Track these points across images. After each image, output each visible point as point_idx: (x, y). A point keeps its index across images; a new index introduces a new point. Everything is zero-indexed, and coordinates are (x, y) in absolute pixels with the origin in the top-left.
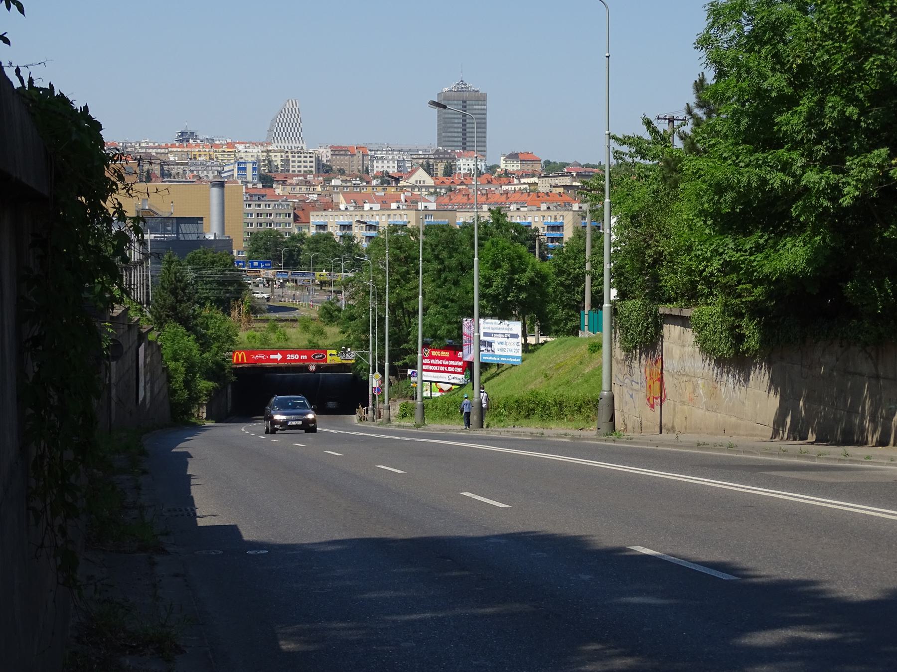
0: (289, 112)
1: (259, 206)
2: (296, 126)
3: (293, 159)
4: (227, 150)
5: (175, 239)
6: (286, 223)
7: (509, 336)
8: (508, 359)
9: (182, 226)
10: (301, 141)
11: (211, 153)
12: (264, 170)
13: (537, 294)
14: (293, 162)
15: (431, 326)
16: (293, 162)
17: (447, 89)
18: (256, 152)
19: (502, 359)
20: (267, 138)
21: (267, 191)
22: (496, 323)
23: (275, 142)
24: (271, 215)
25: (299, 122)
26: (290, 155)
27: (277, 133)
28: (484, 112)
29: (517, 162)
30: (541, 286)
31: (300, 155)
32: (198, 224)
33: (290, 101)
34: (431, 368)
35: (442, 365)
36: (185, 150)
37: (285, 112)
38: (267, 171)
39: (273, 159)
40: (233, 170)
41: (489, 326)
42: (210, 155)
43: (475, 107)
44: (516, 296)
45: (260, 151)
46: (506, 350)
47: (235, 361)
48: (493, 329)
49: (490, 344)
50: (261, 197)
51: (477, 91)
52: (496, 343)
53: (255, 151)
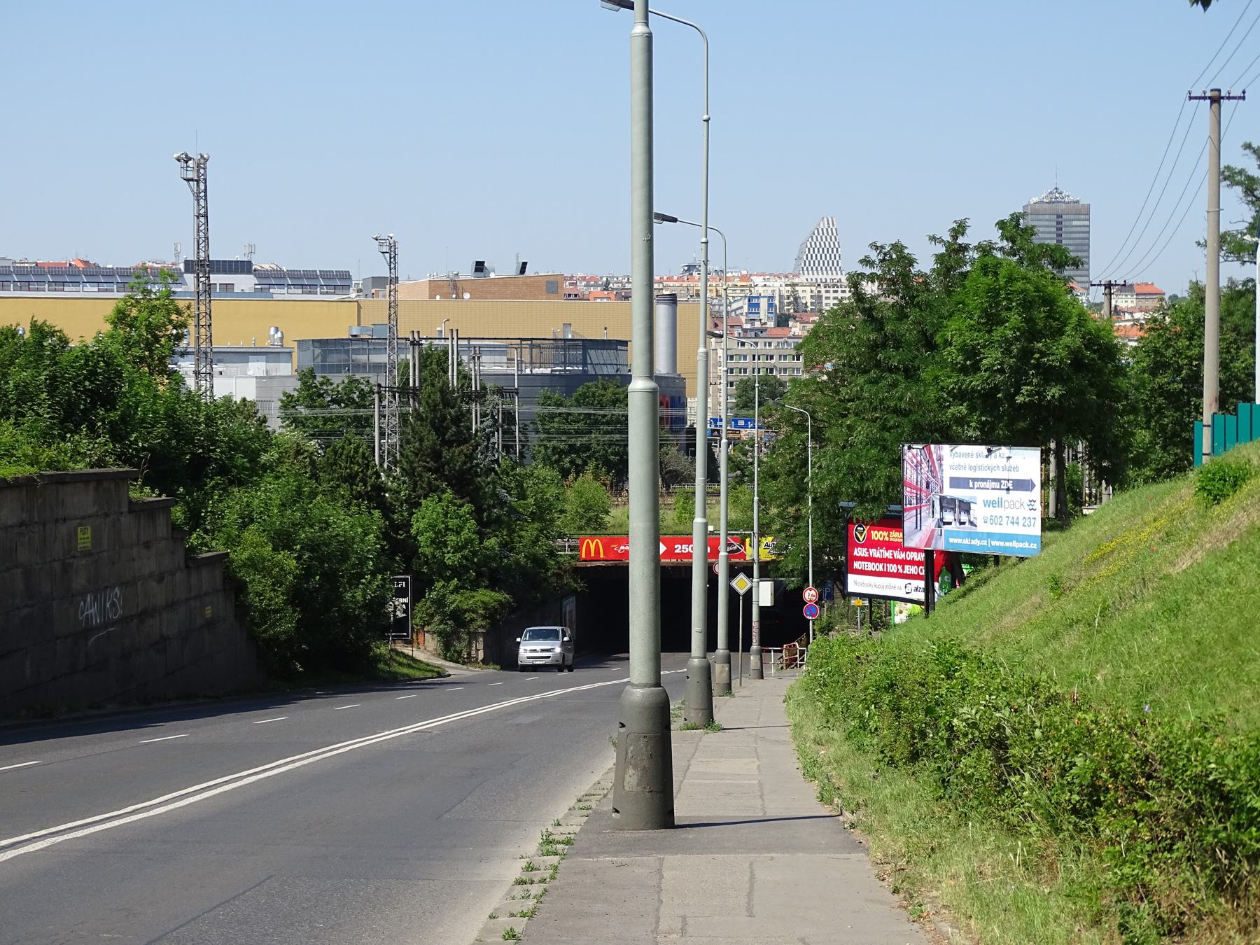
0: (823, 234)
1: (756, 344)
2: (833, 252)
3: (828, 295)
4: (739, 284)
5: (580, 373)
6: (767, 356)
7: (1010, 485)
8: (1008, 544)
9: (592, 352)
10: (839, 272)
11: (718, 288)
12: (789, 310)
13: (1090, 389)
14: (827, 298)
15: (851, 470)
16: (827, 298)
17: (1035, 200)
18: (778, 286)
19: (994, 543)
20: (795, 269)
21: (780, 331)
22: (979, 455)
23: (804, 274)
24: (772, 357)
25: (837, 246)
26: (823, 290)
27: (807, 262)
28: (1087, 229)
29: (1132, 296)
30: (1100, 372)
31: (836, 289)
32: (617, 350)
33: (825, 219)
34: (870, 566)
35: (894, 561)
36: (685, 284)
37: (819, 234)
38: (792, 311)
39: (801, 294)
40: (742, 307)
41: (961, 461)
42: (717, 291)
43: (1074, 223)
44: (1038, 393)
45: (784, 285)
46: (1004, 522)
47: (583, 556)
48: (973, 468)
49: (965, 507)
50: (759, 333)
51: (1077, 202)
52: (981, 504)
53: (777, 284)
